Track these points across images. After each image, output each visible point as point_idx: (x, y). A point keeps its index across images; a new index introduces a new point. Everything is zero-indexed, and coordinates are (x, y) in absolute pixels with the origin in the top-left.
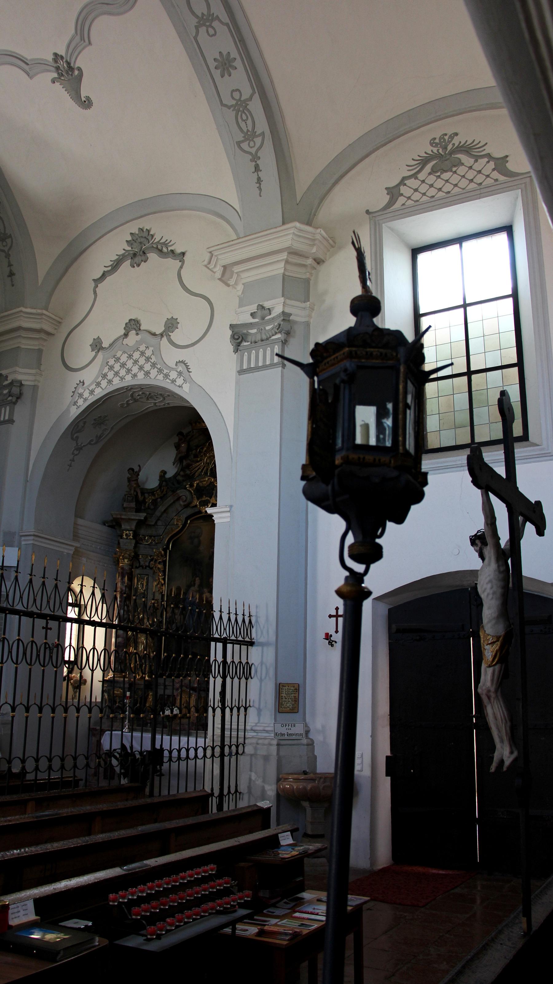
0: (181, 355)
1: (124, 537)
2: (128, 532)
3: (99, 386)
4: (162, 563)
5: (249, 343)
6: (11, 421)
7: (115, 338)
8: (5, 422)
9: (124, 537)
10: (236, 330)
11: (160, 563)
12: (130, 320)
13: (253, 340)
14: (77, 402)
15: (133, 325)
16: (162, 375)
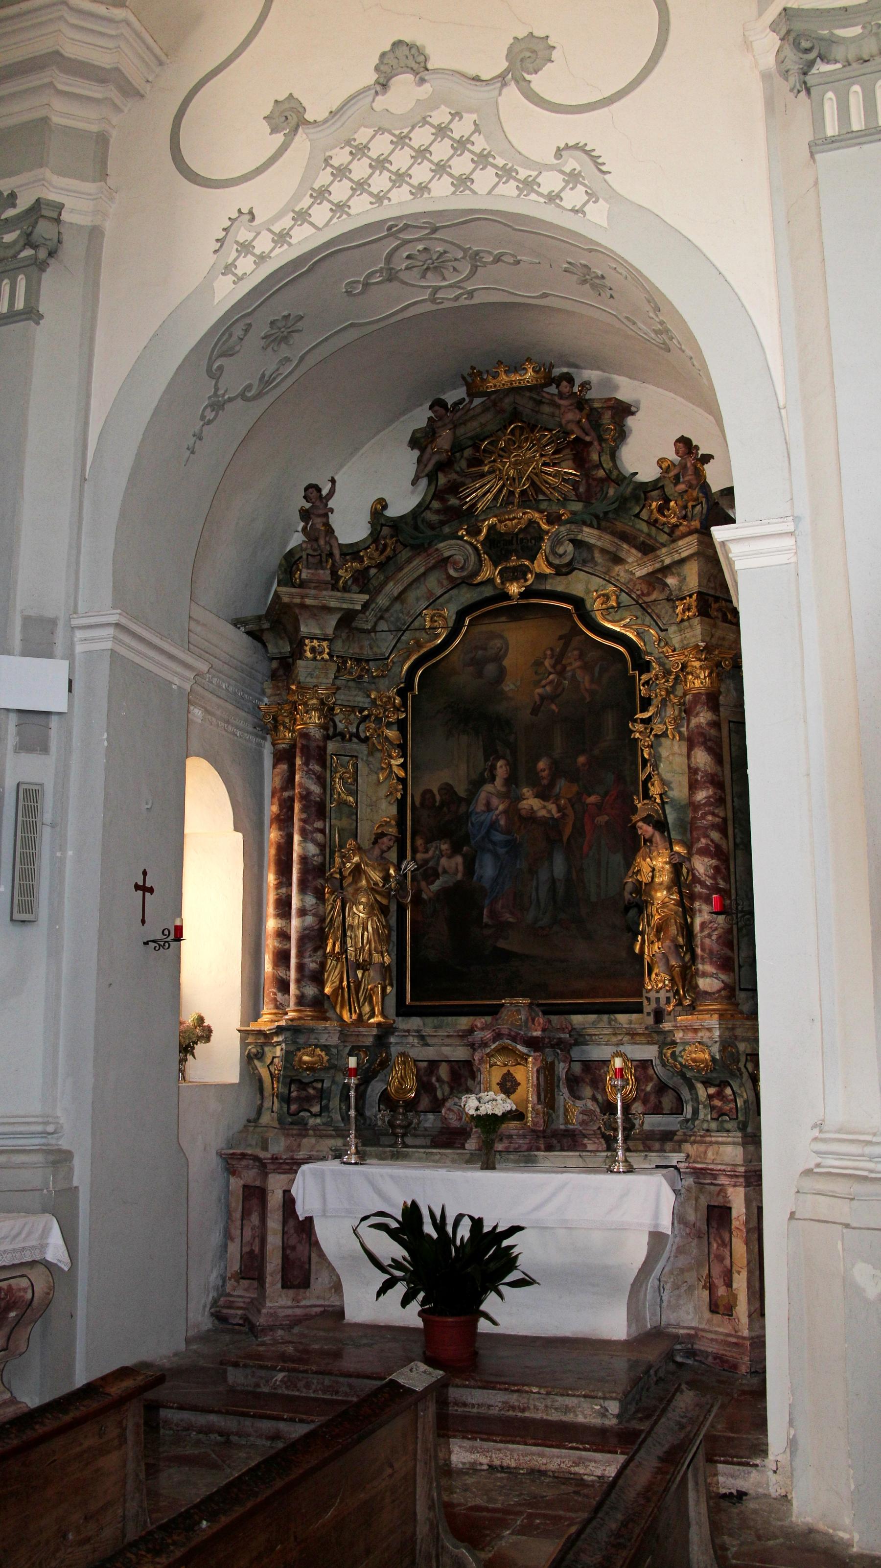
0: (573, 129)
1: (309, 655)
2: (315, 643)
3: (304, 221)
4: (395, 727)
5: (838, 66)
6: (32, 314)
7: (352, 91)
8: (11, 317)
9: (309, 655)
10: (799, 26)
11: (389, 725)
12: (397, 44)
13: (851, 56)
14: (233, 265)
15: (404, 59)
16: (513, 184)
